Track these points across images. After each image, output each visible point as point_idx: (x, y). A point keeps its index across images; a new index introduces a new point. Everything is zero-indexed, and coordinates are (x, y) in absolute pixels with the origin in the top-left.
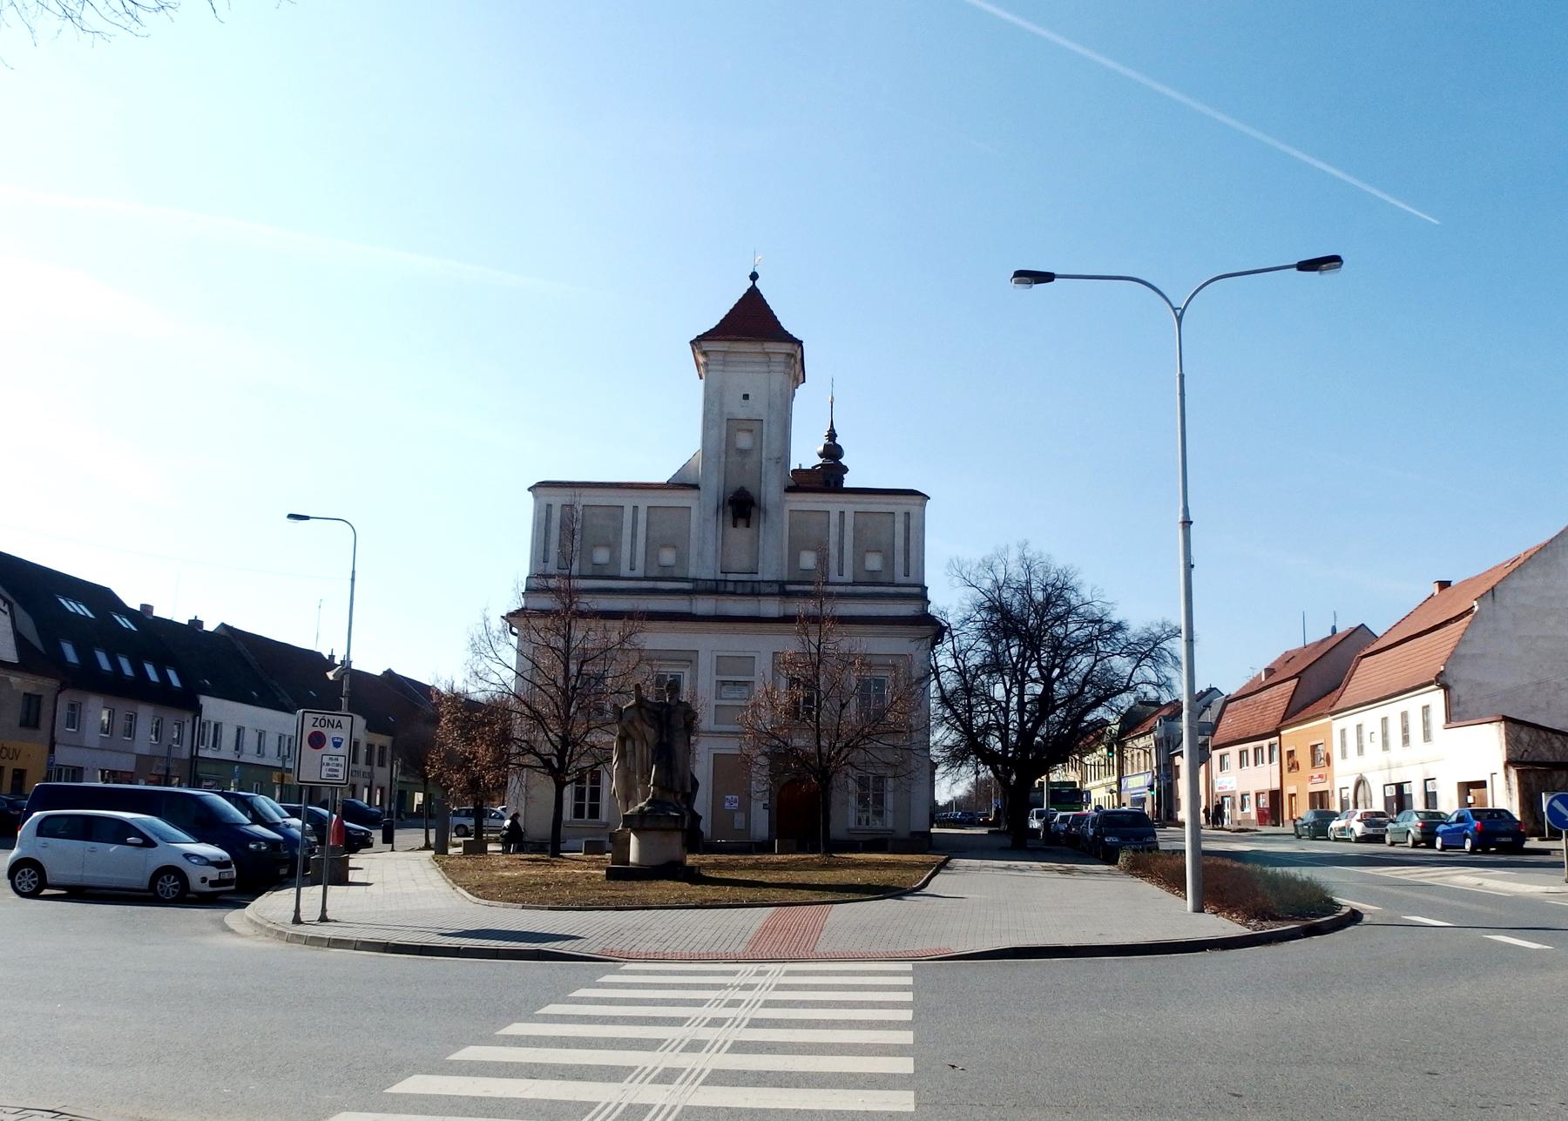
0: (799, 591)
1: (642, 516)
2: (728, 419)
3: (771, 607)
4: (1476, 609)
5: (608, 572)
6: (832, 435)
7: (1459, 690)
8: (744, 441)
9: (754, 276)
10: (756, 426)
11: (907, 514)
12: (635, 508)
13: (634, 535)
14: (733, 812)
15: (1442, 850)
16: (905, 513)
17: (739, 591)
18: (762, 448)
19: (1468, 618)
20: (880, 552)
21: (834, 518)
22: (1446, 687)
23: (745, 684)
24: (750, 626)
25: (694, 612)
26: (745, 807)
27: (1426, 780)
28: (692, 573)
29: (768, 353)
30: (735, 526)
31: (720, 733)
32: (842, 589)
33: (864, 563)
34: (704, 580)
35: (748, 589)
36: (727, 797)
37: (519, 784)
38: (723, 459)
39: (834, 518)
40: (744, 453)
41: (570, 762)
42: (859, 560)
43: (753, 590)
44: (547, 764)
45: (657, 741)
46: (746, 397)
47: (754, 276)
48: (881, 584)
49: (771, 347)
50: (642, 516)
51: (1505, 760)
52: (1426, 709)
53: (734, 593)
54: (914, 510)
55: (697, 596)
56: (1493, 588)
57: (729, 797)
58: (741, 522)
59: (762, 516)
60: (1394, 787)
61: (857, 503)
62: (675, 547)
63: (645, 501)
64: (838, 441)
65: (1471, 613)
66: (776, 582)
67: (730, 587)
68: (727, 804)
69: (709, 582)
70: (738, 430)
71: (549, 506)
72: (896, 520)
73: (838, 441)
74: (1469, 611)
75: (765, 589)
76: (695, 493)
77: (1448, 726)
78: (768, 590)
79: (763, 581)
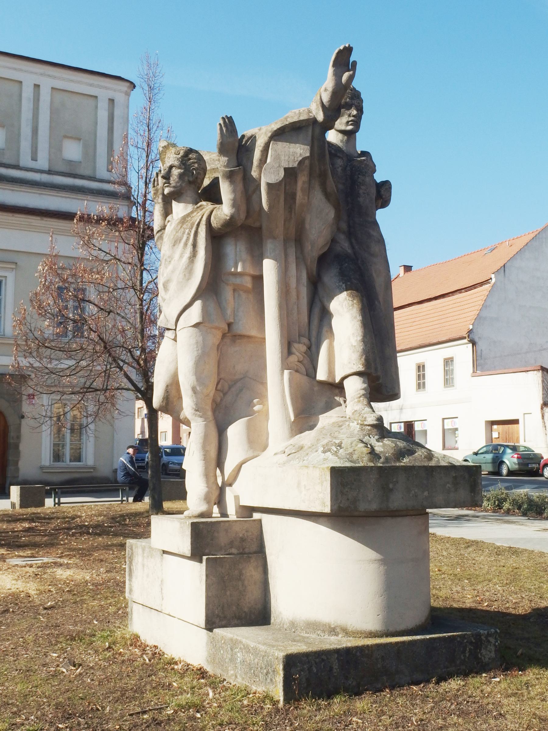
4: (494, 280)
7: (481, 345)
11: (112, 101)
15: (508, 475)
16: (109, 99)
19: (487, 287)
20: (79, 139)
21: (28, 92)
22: (474, 343)
27: (444, 419)
32: (37, 177)
39: (28, 92)
45: (326, 249)
48: (82, 177)
51: (542, 403)
52: (448, 362)
54: (119, 98)
56: (504, 266)
60: (402, 424)
61: (55, 77)
65: (489, 283)
72: (99, 105)
74: (487, 282)
77: (474, 374)
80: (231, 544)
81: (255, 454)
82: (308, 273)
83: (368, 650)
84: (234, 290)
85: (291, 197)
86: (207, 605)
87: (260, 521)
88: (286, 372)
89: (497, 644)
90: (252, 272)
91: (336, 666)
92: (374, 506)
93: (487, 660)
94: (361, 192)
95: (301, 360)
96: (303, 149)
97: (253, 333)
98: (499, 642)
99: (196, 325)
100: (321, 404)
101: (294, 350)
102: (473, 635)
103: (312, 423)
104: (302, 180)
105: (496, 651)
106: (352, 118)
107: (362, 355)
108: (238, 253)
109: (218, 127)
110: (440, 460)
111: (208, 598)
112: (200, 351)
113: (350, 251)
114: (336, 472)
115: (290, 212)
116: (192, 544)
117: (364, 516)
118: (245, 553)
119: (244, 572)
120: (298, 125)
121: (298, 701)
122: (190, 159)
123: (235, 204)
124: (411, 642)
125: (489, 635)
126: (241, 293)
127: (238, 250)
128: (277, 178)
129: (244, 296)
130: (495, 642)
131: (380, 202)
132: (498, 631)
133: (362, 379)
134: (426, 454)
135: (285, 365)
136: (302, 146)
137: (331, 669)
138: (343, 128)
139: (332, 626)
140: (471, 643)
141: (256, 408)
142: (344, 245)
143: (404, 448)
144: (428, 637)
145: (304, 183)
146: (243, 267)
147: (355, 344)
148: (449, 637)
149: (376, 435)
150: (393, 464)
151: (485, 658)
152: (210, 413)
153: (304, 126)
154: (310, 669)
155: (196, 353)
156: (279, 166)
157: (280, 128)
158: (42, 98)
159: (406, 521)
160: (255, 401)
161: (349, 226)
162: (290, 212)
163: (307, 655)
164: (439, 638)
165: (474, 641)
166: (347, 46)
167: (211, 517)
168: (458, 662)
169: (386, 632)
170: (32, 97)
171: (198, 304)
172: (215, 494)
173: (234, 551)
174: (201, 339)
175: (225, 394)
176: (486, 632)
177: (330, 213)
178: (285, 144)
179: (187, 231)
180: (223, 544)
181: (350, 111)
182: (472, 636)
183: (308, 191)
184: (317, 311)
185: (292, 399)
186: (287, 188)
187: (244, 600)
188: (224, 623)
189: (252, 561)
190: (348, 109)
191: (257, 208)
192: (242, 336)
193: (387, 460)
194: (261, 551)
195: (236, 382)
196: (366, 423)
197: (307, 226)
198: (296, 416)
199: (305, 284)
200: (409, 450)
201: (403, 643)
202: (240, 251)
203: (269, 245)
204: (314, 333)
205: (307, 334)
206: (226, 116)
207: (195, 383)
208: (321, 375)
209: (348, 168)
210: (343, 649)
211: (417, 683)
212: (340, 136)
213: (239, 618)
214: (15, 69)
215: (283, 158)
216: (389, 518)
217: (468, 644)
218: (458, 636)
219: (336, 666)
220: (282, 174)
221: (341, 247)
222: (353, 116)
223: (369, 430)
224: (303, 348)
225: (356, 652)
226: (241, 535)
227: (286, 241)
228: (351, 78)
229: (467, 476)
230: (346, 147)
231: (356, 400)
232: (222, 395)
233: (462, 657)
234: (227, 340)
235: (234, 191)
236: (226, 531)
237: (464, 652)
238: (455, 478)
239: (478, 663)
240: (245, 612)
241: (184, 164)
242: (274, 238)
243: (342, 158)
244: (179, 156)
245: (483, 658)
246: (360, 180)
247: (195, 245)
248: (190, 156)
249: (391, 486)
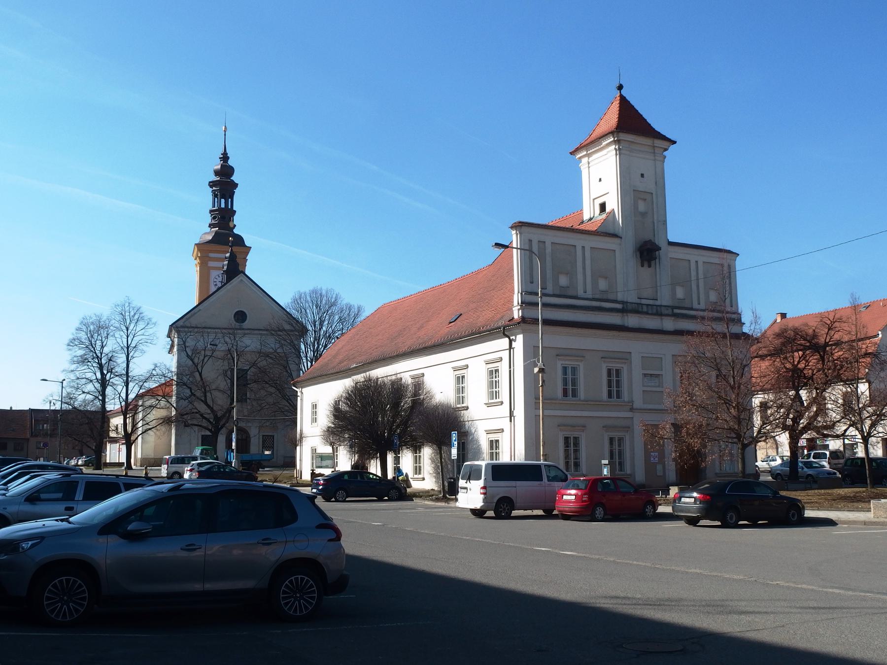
0: (679, 314)
3: (669, 324)
4: (880, 336)
5: (570, 293)
6: (225, 157)
13: (584, 268)
23: (657, 376)
24: (656, 336)
25: (626, 325)
28: (620, 297)
30: (642, 266)
31: (650, 410)
33: (558, 282)
34: (630, 303)
35: (655, 311)
40: (643, 214)
42: (595, 284)
43: (658, 312)
46: (642, 175)
53: (647, 313)
55: (629, 314)
62: (606, 278)
64: (230, 162)
67: (645, 309)
68: (652, 459)
69: (634, 304)
73: (230, 162)
75: (665, 311)
76: (617, 240)
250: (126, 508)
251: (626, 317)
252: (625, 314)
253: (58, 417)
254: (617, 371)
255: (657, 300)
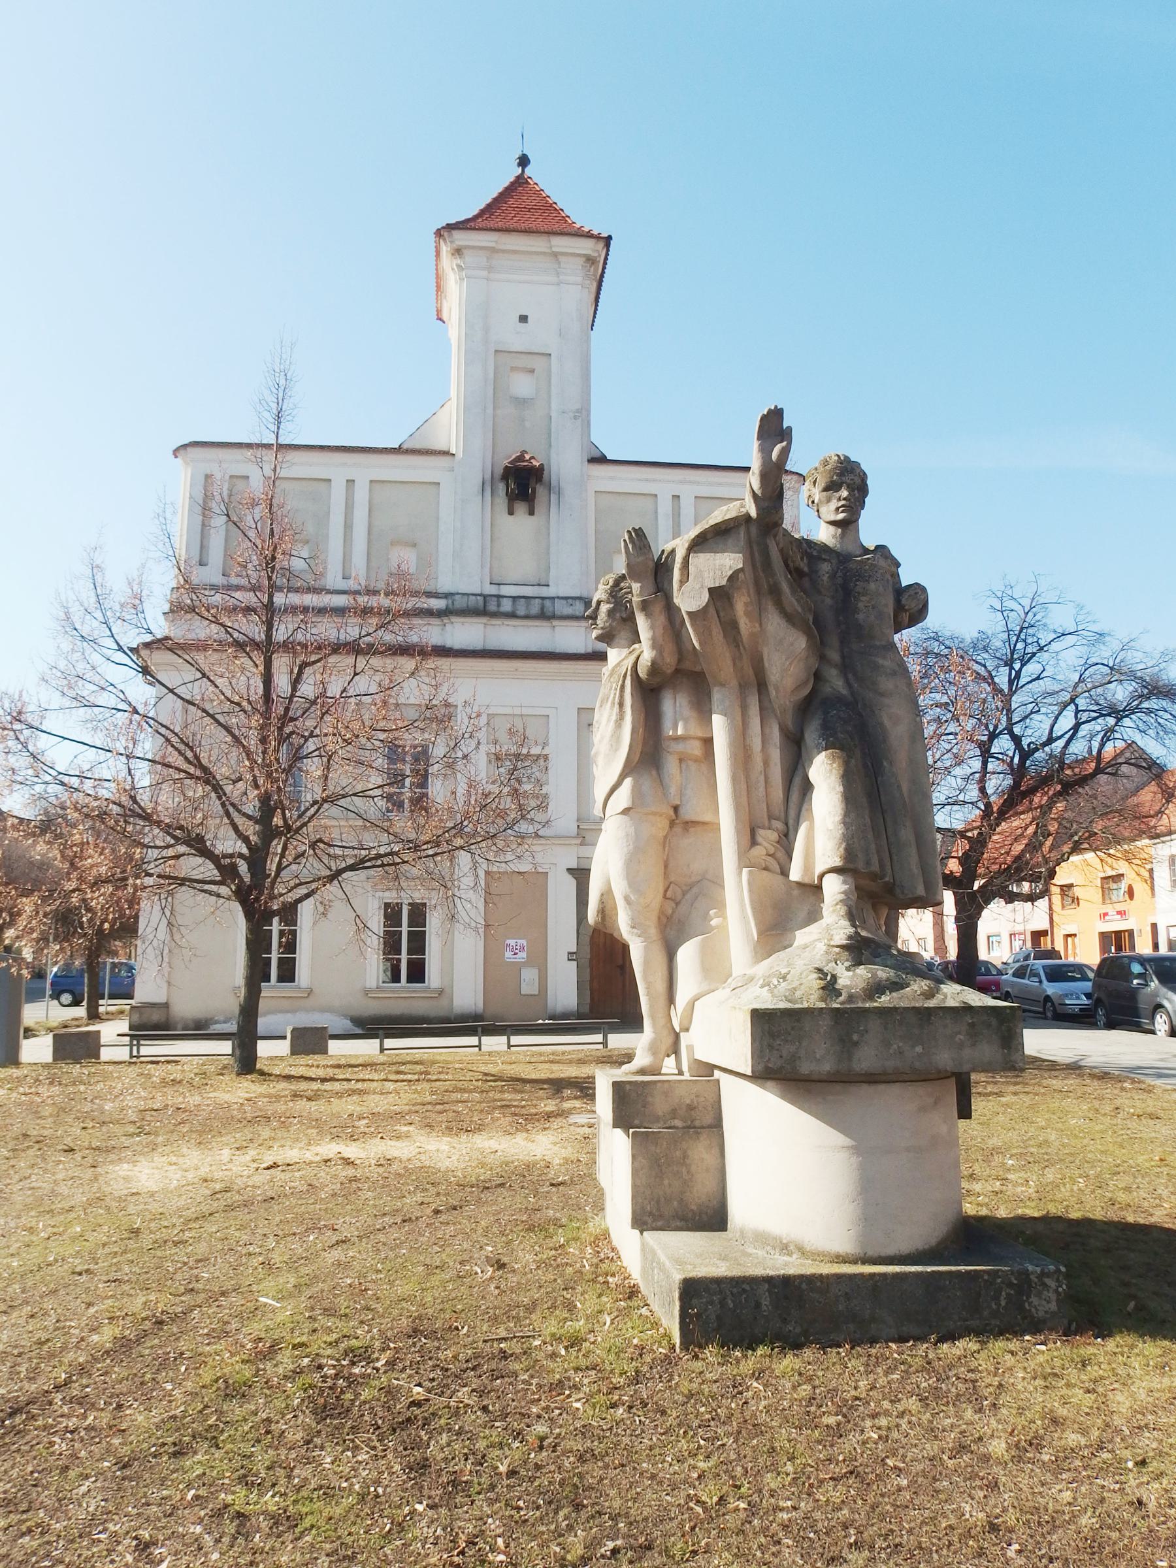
1: (361, 495)
2: (496, 351)
8: (522, 386)
9: (524, 161)
10: (538, 364)
12: (350, 482)
13: (348, 526)
14: (518, 967)
17: (521, 612)
18: (549, 397)
26: (539, 959)
28: (445, 583)
29: (555, 255)
30: (511, 512)
35: (535, 608)
36: (508, 942)
37: (164, 922)
38: (490, 411)
40: (522, 403)
41: (280, 869)
44: (228, 872)
45: (806, 691)
47: (524, 161)
49: (561, 244)
50: (361, 495)
53: (512, 615)
57: (512, 942)
58: (521, 508)
59: (553, 497)
61: (698, 483)
63: (366, 470)
66: (580, 598)
67: (507, 606)
68: (508, 954)
70: (513, 369)
71: (208, 477)
75: (561, 608)
78: (568, 611)
79: (558, 597)
80: (674, 1113)
81: (712, 987)
82: (781, 729)
83: (822, 1282)
84: (681, 760)
85: (731, 628)
86: (634, 1197)
87: (718, 1081)
88: (745, 870)
89: (1060, 1289)
90: (700, 734)
91: (766, 1302)
92: (827, 1067)
93: (1041, 1314)
94: (861, 605)
95: (772, 852)
96: (734, 559)
97: (707, 818)
98: (1065, 1287)
99: (625, 812)
100: (802, 915)
101: (759, 839)
102: (1012, 1273)
103: (787, 943)
104: (741, 604)
105: (1058, 1300)
106: (843, 502)
107: (841, 843)
108: (678, 709)
109: (623, 544)
110: (949, 997)
111: (634, 1187)
112: (631, 847)
113: (845, 692)
114: (760, 1018)
115: (738, 646)
116: (614, 1112)
117: (826, 1081)
118: (694, 1127)
119: (690, 1153)
120: (723, 527)
121: (701, 1347)
122: (622, 589)
123: (655, 645)
124: (896, 1276)
125: (1043, 1274)
126: (690, 763)
127: (678, 704)
128: (699, 603)
129: (693, 767)
130: (1058, 1287)
131: (906, 618)
132: (1063, 1269)
133: (841, 878)
134: (926, 988)
135: (744, 860)
136: (733, 555)
137: (758, 1305)
138: (833, 518)
139: (785, 1241)
140: (1010, 1285)
141: (714, 923)
142: (836, 683)
143: (888, 979)
144: (929, 1269)
145: (746, 604)
146: (685, 728)
147: (831, 827)
148: (968, 1272)
149: (847, 960)
150: (860, 1005)
151: (1037, 1310)
152: (653, 931)
153: (731, 528)
154: (722, 1302)
155: (625, 849)
156: (702, 587)
157: (701, 533)
158: (683, 512)
159: (895, 1089)
160: (712, 912)
161: (843, 657)
162: (738, 646)
163: (718, 1281)
164: (950, 1272)
165: (1015, 1282)
166: (773, 408)
167: (660, 1074)
168: (986, 1313)
169: (862, 1255)
170: (671, 513)
171: (628, 782)
172: (669, 1041)
173: (678, 1123)
174: (632, 830)
175: (677, 904)
176: (1038, 1269)
177: (800, 642)
178: (708, 555)
179: (614, 685)
180: (660, 1114)
181: (840, 493)
182: (1012, 1273)
183: (758, 616)
184: (797, 781)
185: (754, 909)
186: (722, 614)
187: (691, 1193)
188: (659, 1224)
189: (701, 1139)
190: (837, 491)
191: (691, 648)
192: (695, 823)
193: (851, 998)
194: (717, 1125)
195: (691, 886)
196: (832, 943)
197: (766, 665)
198: (760, 934)
199: (778, 744)
200: (895, 983)
201: (884, 1276)
202: (680, 706)
203: (717, 695)
204: (792, 813)
205: (783, 814)
206: (633, 528)
207: (628, 890)
208: (795, 874)
209: (840, 574)
210: (779, 1276)
211: (902, 1340)
212: (832, 529)
213: (683, 1219)
214: (647, 480)
215: (706, 575)
216: (865, 1086)
217: (1004, 1286)
218: (984, 1271)
219: (766, 1302)
220: (706, 597)
221: (832, 687)
222: (844, 499)
223: (837, 954)
224: (774, 836)
225: (801, 1283)
226: (688, 1102)
227: (743, 687)
228: (785, 452)
229: (994, 1022)
230: (840, 543)
231: (831, 909)
232: (674, 905)
233: (994, 1306)
234: (678, 829)
235: (652, 627)
236: (666, 1094)
237: (997, 1298)
238: (972, 1025)
239: (1024, 1318)
240: (692, 1210)
241: (613, 597)
242: (722, 685)
243: (829, 561)
244: (608, 587)
245: (1033, 1310)
246: (858, 589)
247: (621, 705)
248: (622, 584)
249: (855, 1037)
250: (737, 820)
251: (448, 627)
252: (446, 620)
253: (1019, 881)
254: (396, 978)
255: (548, 585)
